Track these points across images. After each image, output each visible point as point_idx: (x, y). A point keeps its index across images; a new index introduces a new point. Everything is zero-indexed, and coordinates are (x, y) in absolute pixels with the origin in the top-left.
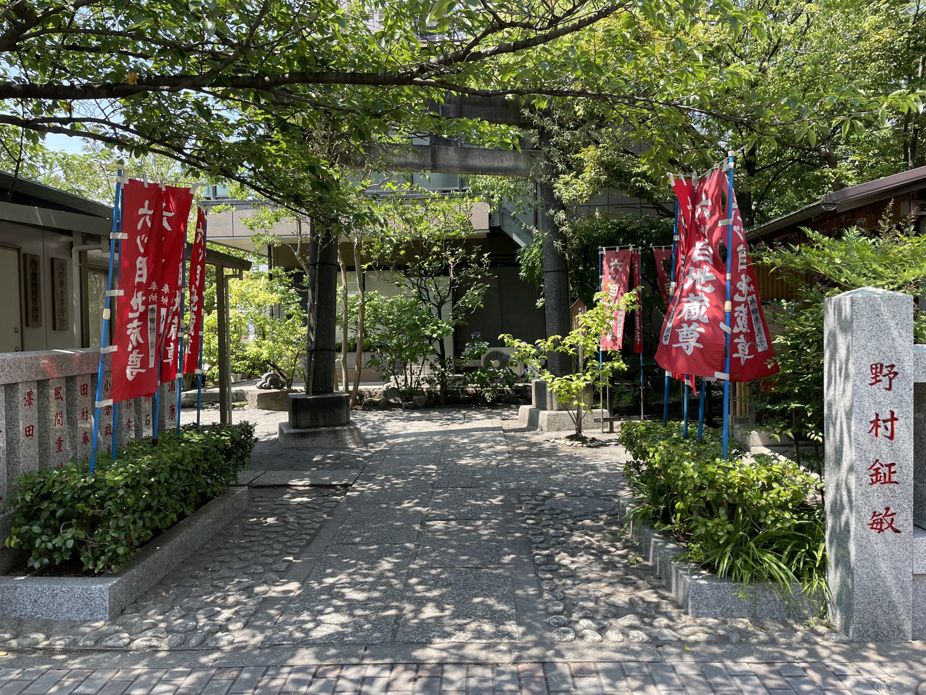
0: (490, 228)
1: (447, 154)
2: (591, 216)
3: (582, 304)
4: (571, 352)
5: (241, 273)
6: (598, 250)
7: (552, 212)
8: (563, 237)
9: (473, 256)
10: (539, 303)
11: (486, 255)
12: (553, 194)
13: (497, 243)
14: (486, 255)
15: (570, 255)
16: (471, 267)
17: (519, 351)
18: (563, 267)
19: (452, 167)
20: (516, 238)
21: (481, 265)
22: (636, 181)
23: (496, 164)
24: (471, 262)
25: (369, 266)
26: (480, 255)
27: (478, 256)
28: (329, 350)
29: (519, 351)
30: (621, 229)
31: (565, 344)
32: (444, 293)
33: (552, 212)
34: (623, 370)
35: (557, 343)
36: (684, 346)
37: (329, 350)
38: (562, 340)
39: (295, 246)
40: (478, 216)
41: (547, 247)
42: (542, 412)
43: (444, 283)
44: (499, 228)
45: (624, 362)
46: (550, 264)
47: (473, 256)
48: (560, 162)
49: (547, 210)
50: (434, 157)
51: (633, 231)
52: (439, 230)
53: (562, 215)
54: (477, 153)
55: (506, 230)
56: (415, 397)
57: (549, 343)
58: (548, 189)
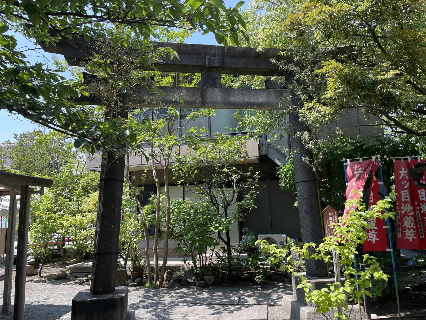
0: (260, 156)
1: (213, 93)
2: (334, 136)
3: (332, 209)
4: (326, 260)
5: (42, 189)
6: (343, 162)
7: (298, 133)
8: (309, 152)
9: (249, 174)
10: (296, 205)
11: (257, 173)
12: (298, 118)
13: (265, 165)
14: (257, 173)
15: (317, 168)
16: (247, 181)
17: (275, 257)
18: (312, 178)
19: (217, 102)
20: (277, 162)
21: (254, 180)
22: (382, 88)
23: (253, 100)
24: (247, 178)
25: (182, 182)
26: (253, 173)
27: (252, 174)
28: (110, 254)
29: (275, 257)
30: (357, 147)
31: (320, 252)
32: (229, 198)
33: (298, 133)
34: (382, 280)
35: (311, 250)
36: (408, 238)
37: (110, 254)
38: (317, 247)
39: (143, 172)
40: (251, 149)
41: (297, 162)
42: (302, 308)
43: (228, 193)
44: (266, 156)
45: (385, 272)
46: (300, 176)
47: (249, 174)
48: (303, 94)
49: (295, 133)
50: (203, 96)
51: (369, 148)
52: (168, 137)
53: (306, 135)
54: (237, 92)
55: (271, 156)
56: (206, 277)
57: (304, 250)
58: (294, 117)
